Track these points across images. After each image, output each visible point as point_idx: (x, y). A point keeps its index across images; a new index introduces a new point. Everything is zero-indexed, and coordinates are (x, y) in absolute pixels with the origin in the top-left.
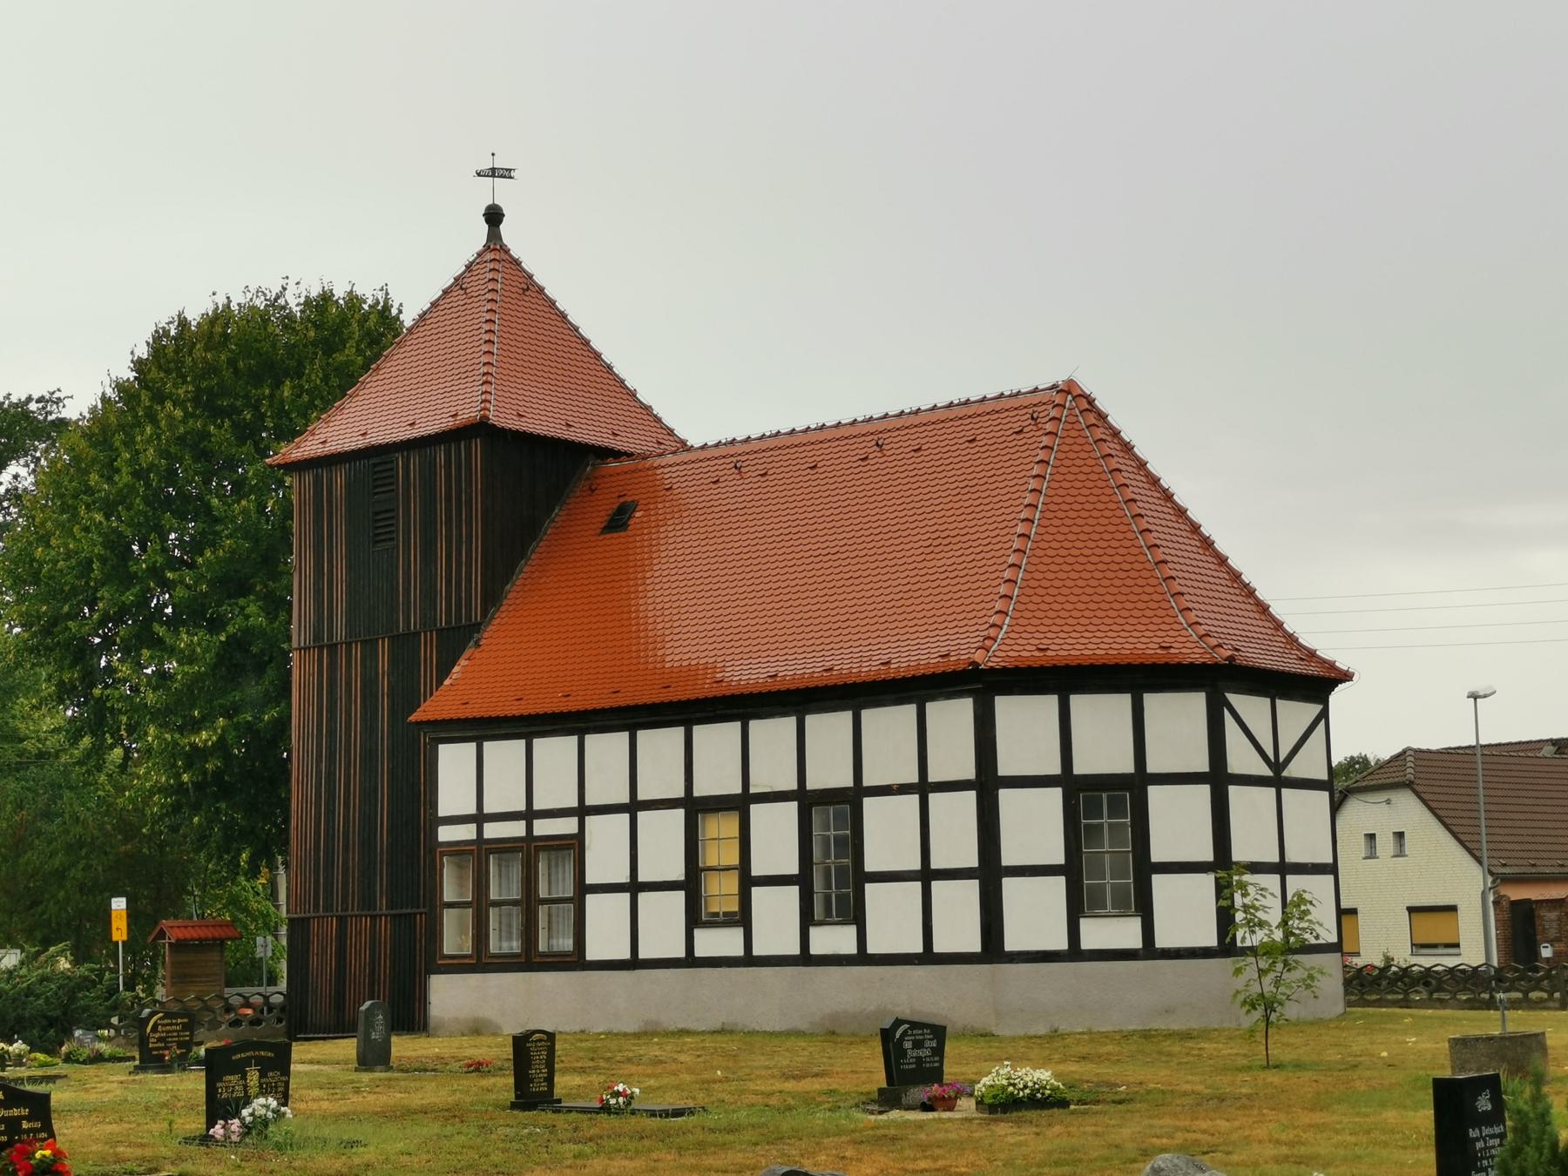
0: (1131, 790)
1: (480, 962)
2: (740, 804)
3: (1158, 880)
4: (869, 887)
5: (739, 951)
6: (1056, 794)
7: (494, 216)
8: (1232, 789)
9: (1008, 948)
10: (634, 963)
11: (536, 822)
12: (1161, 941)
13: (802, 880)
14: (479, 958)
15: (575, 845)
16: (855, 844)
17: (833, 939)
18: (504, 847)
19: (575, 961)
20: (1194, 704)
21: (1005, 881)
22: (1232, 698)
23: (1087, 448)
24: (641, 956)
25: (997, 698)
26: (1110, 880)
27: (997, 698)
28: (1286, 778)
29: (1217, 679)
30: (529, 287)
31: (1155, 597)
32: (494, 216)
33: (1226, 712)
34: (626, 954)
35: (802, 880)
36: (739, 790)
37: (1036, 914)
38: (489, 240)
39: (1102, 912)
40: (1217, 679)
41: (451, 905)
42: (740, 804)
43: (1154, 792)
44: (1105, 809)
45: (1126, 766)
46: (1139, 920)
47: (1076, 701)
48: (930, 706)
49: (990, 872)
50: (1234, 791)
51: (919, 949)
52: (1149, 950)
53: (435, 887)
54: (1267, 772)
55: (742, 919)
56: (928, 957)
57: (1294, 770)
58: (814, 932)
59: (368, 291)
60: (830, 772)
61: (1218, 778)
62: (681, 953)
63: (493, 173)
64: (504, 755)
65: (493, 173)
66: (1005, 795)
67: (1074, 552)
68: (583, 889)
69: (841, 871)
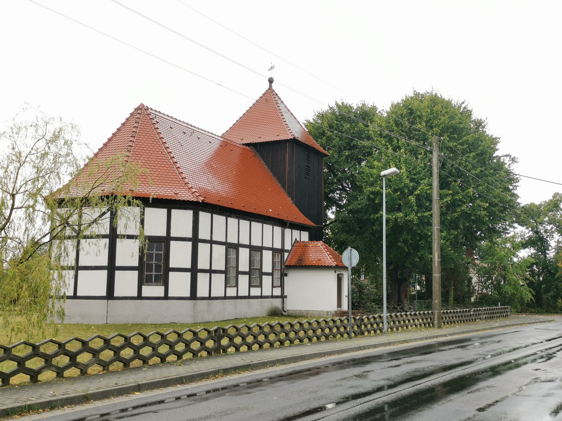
4: (171, 274)
5: (162, 295)
7: (271, 81)
9: (115, 295)
10: (210, 298)
17: (255, 292)
20: (188, 214)
21: (116, 272)
31: (171, 171)
32: (271, 81)
35: (262, 274)
37: (126, 283)
45: (163, 233)
47: (173, 211)
60: (256, 242)
61: (195, 240)
64: (219, 220)
67: (141, 148)
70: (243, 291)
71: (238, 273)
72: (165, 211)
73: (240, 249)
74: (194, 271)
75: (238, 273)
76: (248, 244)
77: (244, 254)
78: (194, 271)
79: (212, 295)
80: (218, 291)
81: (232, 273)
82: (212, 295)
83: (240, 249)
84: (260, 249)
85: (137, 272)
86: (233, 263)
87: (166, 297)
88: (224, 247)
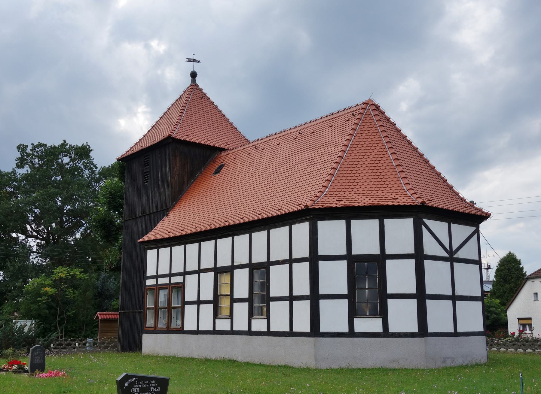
0: (379, 261)
1: (155, 330)
2: (230, 270)
3: (390, 302)
6: (344, 263)
7: (194, 75)
8: (426, 262)
11: (172, 278)
12: (391, 329)
13: (250, 300)
14: (155, 328)
15: (181, 287)
16: (266, 286)
17: (259, 325)
18: (163, 287)
19: (181, 331)
22: (427, 221)
23: (373, 123)
24: (458, 331)
25: (319, 222)
26: (366, 300)
27: (319, 222)
28: (456, 258)
29: (419, 213)
30: (203, 97)
32: (194, 75)
33: (423, 227)
34: (211, 329)
35: (250, 300)
36: (230, 264)
37: (334, 316)
38: (192, 82)
39: (365, 316)
40: (419, 213)
41: (149, 308)
42: (230, 270)
43: (389, 262)
44: (367, 271)
45: (376, 251)
46: (381, 319)
48: (293, 226)
49: (315, 297)
50: (427, 263)
51: (288, 330)
52: (386, 333)
53: (144, 302)
54: (445, 254)
55: (382, 312)
56: (291, 334)
57: (460, 254)
58: (217, 321)
59: (518, 258)
61: (419, 257)
62: (452, 330)
63: (194, 61)
65: (194, 61)
66: (321, 263)
69: (263, 296)
70: (241, 324)
71: (233, 301)
72: (376, 222)
74: (421, 296)
75: (233, 301)
77: (242, 277)
78: (421, 296)
79: (459, 330)
80: (206, 324)
81: (225, 303)
82: (459, 330)
85: (248, 303)
86: (257, 291)
87: (386, 333)
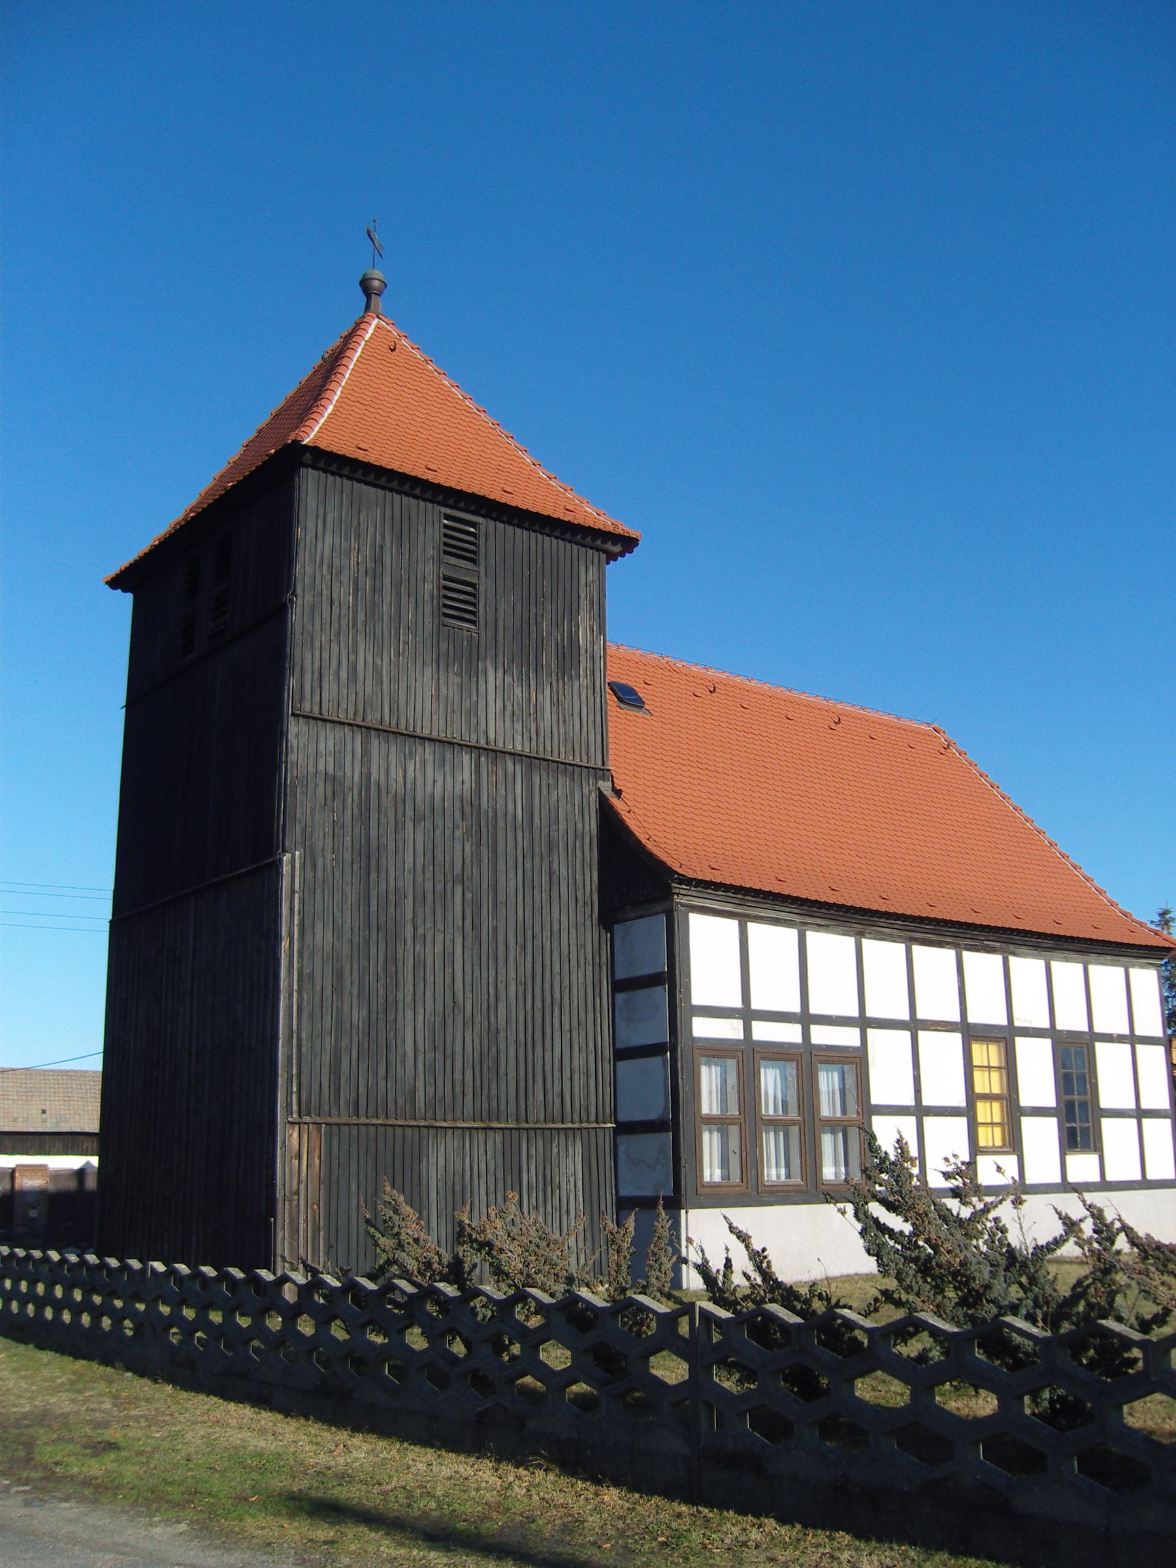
1: (750, 1190)
6: (957, 1037)
15: (855, 1062)
17: (1082, 1167)
18: (776, 1052)
34: (1057, 1179)
60: (987, 1010)
68: (869, 1110)
73: (1019, 1041)
76: (956, 1018)
83: (1019, 1041)
84: (1005, 1036)
88: (1047, 1043)
